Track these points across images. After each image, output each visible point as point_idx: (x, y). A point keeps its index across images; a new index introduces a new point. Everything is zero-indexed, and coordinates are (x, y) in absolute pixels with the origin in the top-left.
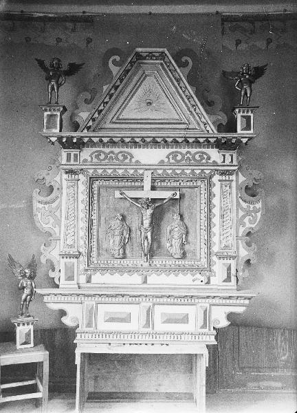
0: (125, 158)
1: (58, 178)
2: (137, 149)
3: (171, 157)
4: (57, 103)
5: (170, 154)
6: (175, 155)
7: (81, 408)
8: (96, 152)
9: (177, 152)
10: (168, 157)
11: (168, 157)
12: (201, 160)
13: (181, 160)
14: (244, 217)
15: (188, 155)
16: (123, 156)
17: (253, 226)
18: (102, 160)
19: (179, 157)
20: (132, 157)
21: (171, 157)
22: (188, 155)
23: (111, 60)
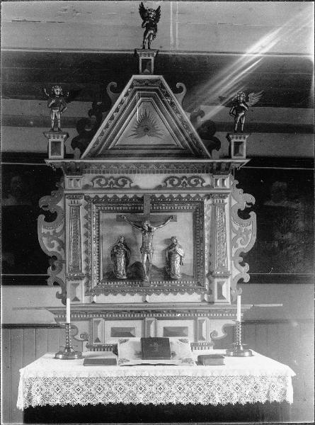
0: (125, 183)
1: (60, 204)
2: (136, 174)
3: (168, 182)
4: (149, 48)
5: (94, 179)
6: (171, 179)
7: (3, 166)
8: (97, 177)
9: (173, 177)
10: (92, 181)
11: (165, 181)
12: (196, 184)
13: (179, 184)
14: (236, 238)
15: (112, 180)
16: (123, 181)
17: (245, 247)
18: (104, 185)
19: (176, 182)
20: (131, 182)
21: (168, 182)
22: (112, 180)
23: (108, 88)
